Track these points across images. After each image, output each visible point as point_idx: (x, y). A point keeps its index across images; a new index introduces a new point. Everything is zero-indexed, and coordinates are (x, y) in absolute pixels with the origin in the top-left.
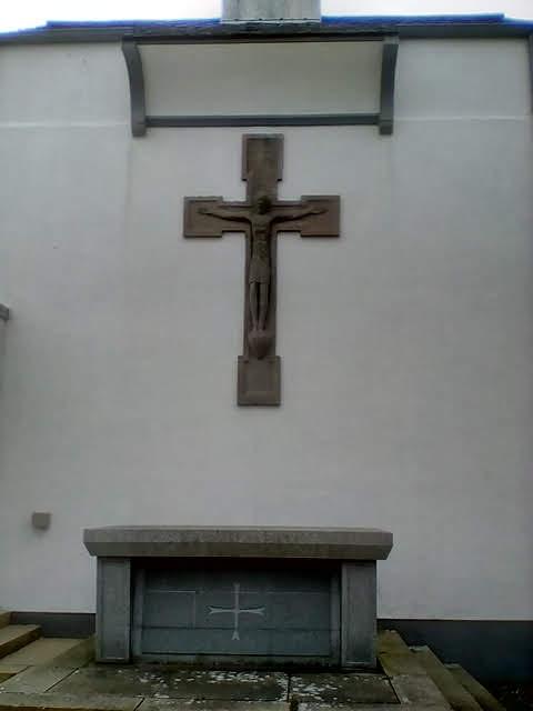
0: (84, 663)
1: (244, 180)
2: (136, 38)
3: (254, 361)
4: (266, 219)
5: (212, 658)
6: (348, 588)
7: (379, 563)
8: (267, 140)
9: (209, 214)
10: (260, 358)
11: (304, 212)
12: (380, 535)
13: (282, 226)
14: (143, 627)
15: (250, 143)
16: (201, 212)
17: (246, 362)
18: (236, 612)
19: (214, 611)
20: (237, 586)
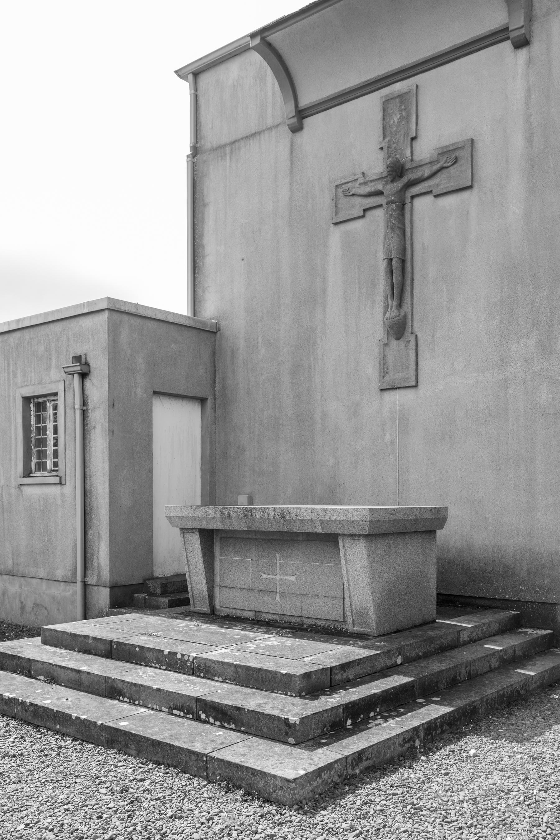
0: (23, 596)
1: (382, 148)
2: (265, 41)
3: (394, 343)
4: (399, 185)
5: (264, 615)
6: (345, 559)
7: (438, 532)
8: (402, 97)
9: (353, 195)
10: (398, 339)
11: (435, 168)
12: (435, 510)
13: (416, 190)
14: (221, 587)
15: (386, 103)
16: (402, 168)
17: (385, 345)
18: (278, 577)
19: (264, 576)
20: (278, 556)
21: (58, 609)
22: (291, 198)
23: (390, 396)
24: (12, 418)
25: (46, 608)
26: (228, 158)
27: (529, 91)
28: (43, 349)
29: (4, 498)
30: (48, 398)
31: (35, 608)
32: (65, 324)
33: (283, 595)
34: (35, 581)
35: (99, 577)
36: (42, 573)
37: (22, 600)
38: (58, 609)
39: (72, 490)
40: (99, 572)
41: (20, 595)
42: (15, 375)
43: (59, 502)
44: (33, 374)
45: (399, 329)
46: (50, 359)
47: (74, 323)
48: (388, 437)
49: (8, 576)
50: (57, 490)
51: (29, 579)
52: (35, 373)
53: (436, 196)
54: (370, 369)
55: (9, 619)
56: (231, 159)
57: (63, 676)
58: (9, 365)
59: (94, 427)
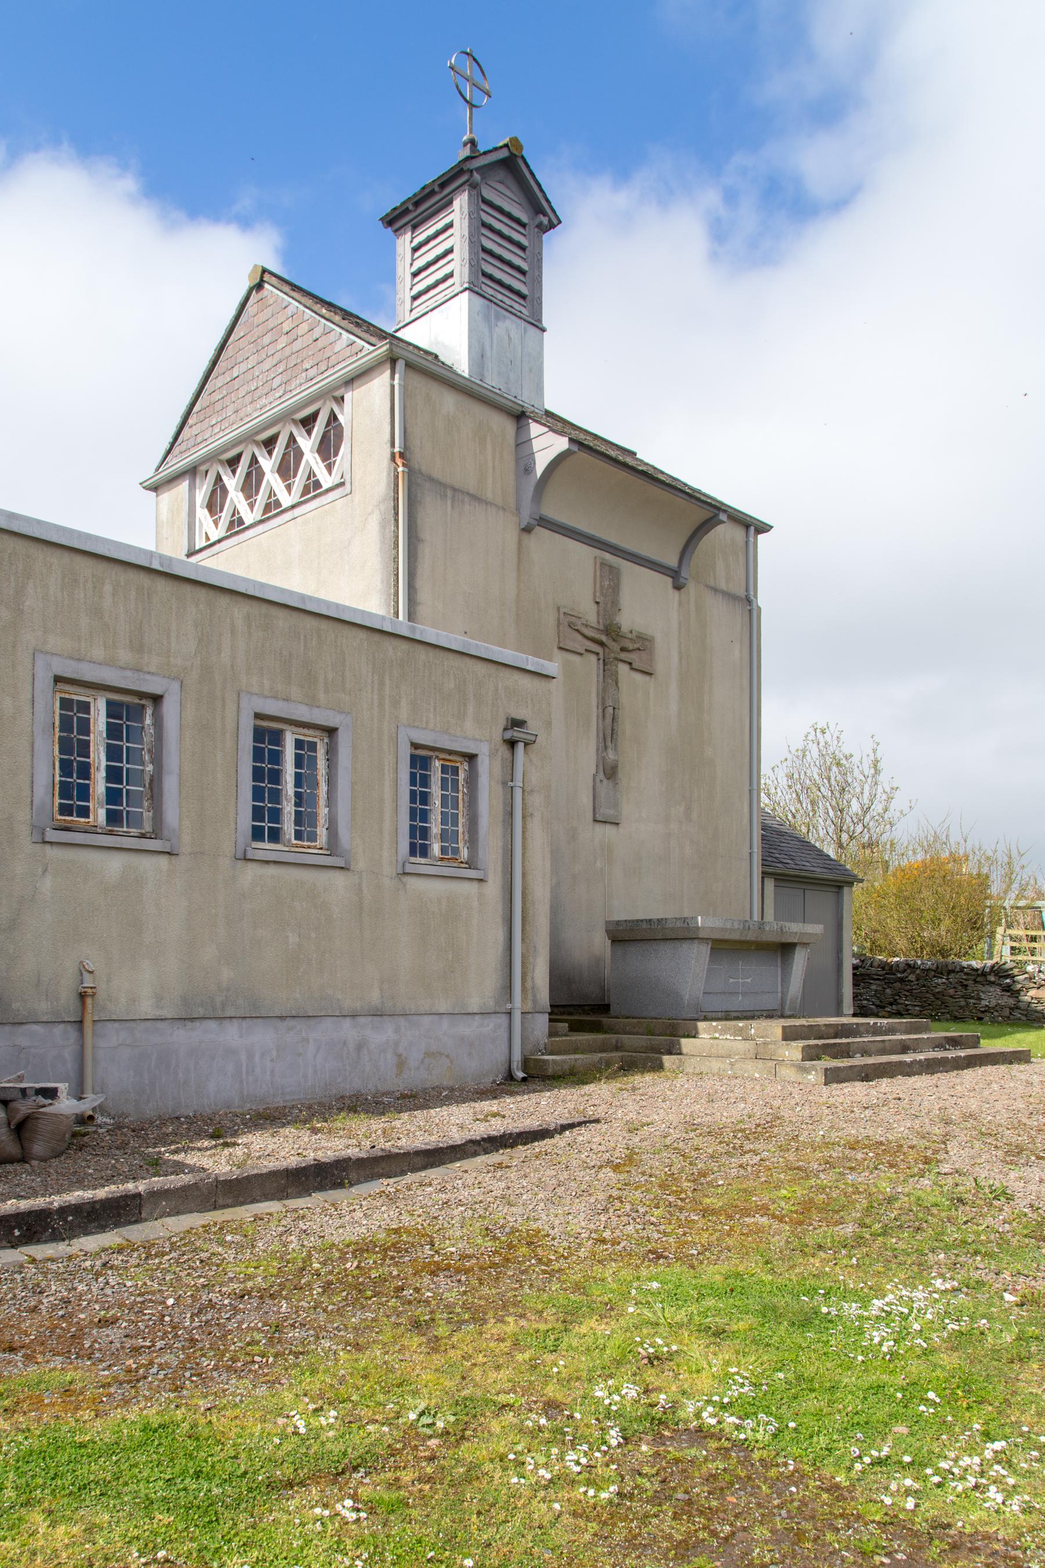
9: (577, 630)
19: (731, 980)
21: (470, 1054)
22: (518, 596)
23: (599, 828)
24: (386, 768)
25: (447, 1056)
26: (449, 502)
27: (680, 623)
28: (452, 685)
29: (365, 892)
30: (437, 753)
31: (426, 1060)
32: (492, 668)
33: (744, 994)
34: (426, 1019)
35: (535, 1001)
36: (443, 1007)
37: (401, 1050)
38: (470, 1054)
39: (493, 888)
40: (534, 996)
41: (397, 1044)
42: (396, 704)
43: (475, 904)
44: (432, 716)
45: (610, 772)
46: (465, 704)
47: (506, 673)
48: (598, 864)
49: (370, 1018)
50: (472, 888)
51: (416, 1018)
52: (435, 715)
53: (632, 669)
54: (585, 799)
55: (370, 1086)
56: (452, 506)
57: (418, 1161)
58: (382, 684)
59: (532, 815)
